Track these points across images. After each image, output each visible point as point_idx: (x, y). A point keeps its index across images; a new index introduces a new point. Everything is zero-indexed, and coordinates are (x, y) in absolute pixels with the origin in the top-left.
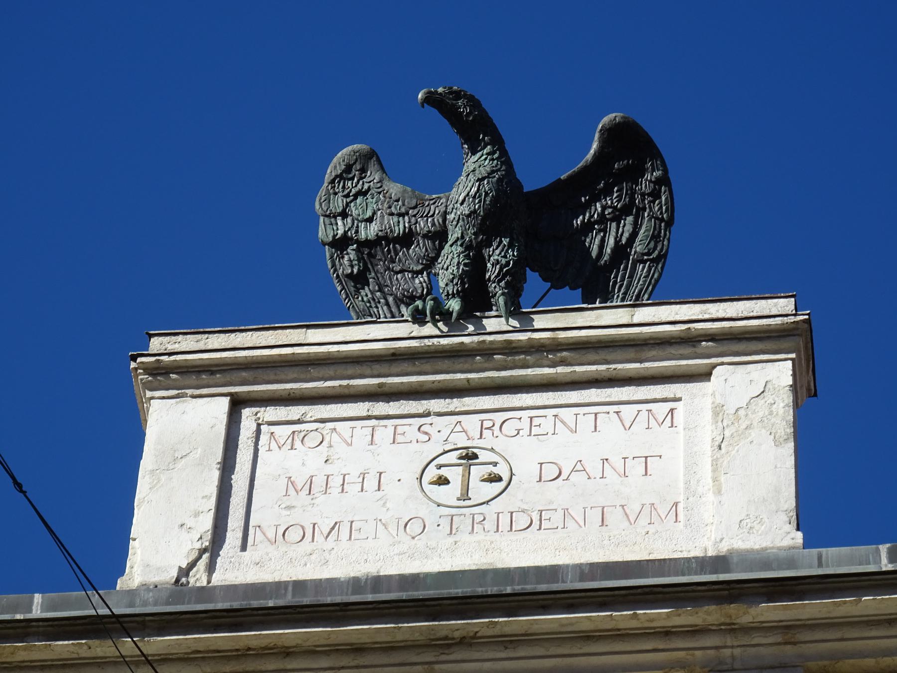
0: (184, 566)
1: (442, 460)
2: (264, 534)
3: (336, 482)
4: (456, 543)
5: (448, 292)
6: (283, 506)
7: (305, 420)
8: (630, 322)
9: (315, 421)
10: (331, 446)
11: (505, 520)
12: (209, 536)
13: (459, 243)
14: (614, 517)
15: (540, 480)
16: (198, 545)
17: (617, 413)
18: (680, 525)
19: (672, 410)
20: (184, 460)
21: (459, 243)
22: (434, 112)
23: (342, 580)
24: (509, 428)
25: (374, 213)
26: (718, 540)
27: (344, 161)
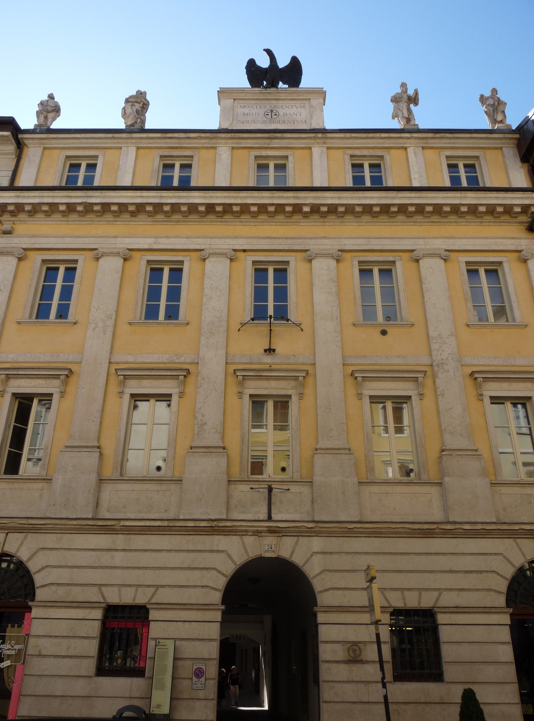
3: (251, 114)
14: (296, 122)
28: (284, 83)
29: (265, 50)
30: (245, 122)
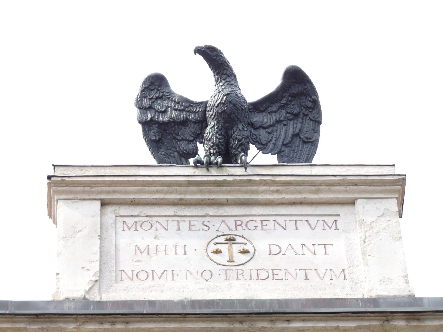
0: (87, 289)
1: (217, 240)
2: (126, 274)
3: (161, 249)
4: (230, 284)
5: (210, 152)
6: (135, 260)
7: (141, 215)
8: (310, 174)
9: (146, 216)
10: (156, 230)
11: (254, 274)
12: (98, 274)
13: (216, 127)
14: (312, 274)
15: (270, 254)
16: (94, 279)
17: (307, 221)
18: (347, 281)
19: (335, 221)
20: (80, 233)
21: (216, 127)
22: (200, 58)
23: (175, 301)
24: (251, 225)
25: (290, 113)
26: (370, 290)
27: (149, 80)
28: (263, 148)
29: (199, 51)
30: (143, 276)
